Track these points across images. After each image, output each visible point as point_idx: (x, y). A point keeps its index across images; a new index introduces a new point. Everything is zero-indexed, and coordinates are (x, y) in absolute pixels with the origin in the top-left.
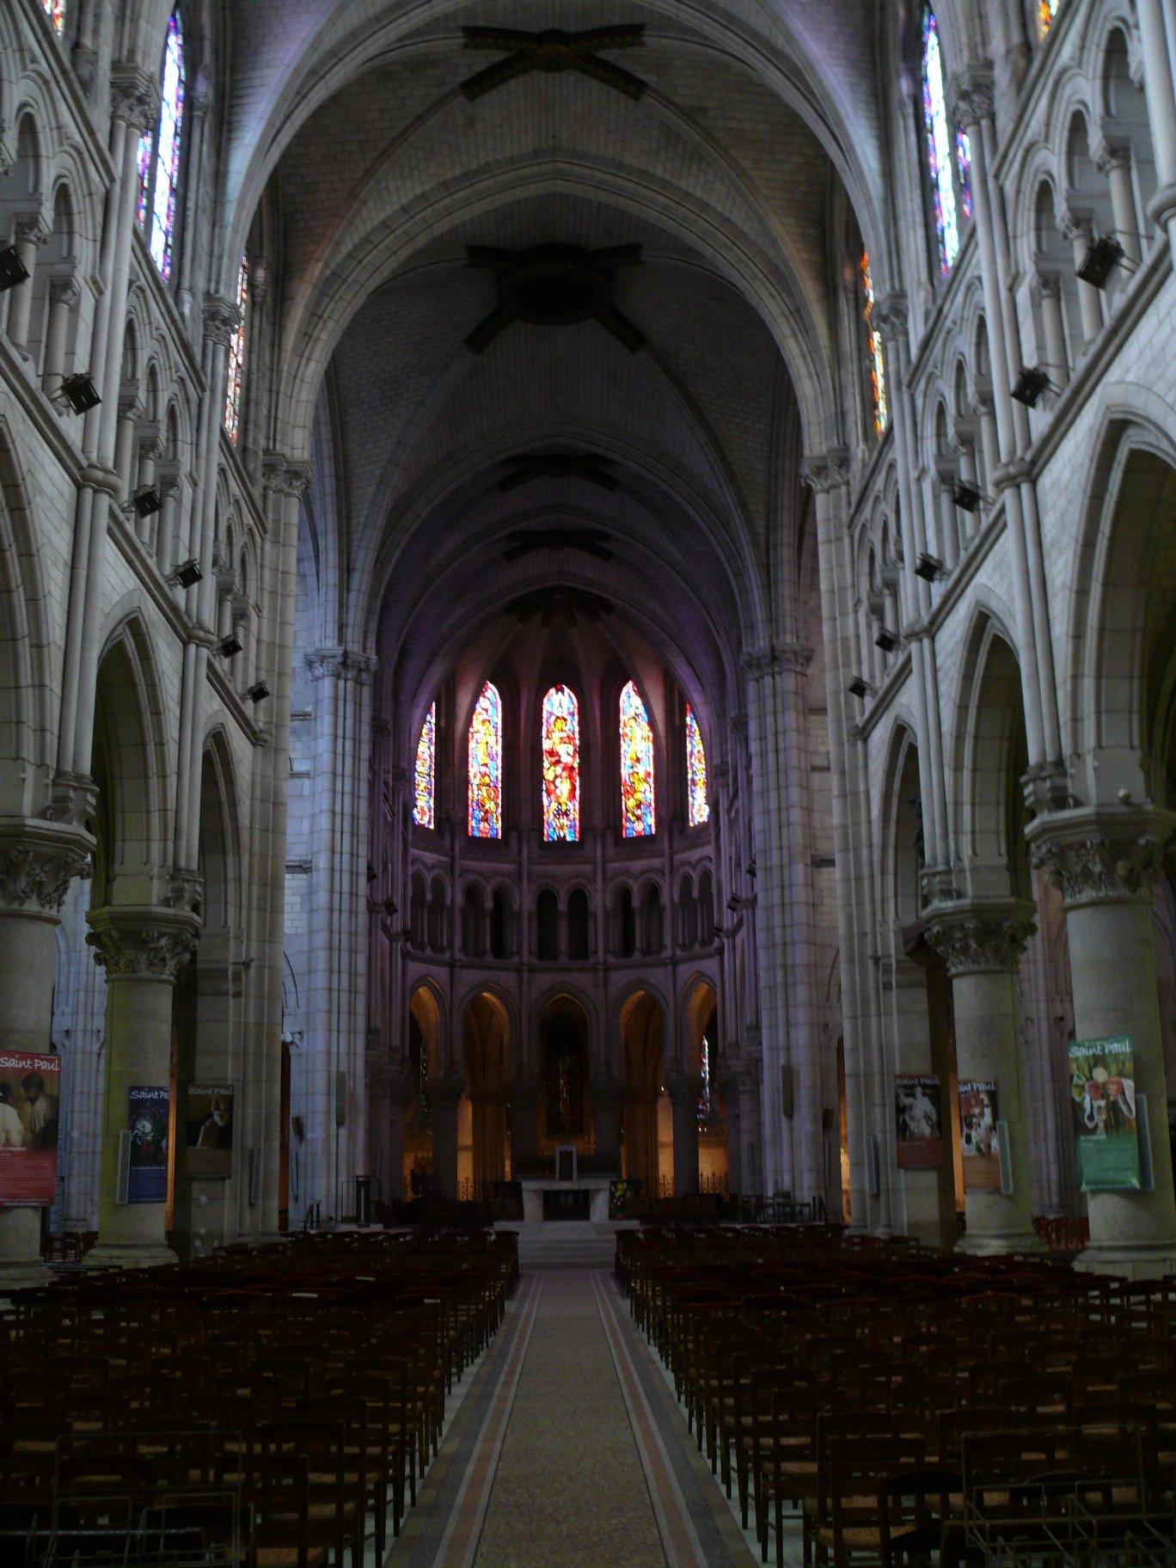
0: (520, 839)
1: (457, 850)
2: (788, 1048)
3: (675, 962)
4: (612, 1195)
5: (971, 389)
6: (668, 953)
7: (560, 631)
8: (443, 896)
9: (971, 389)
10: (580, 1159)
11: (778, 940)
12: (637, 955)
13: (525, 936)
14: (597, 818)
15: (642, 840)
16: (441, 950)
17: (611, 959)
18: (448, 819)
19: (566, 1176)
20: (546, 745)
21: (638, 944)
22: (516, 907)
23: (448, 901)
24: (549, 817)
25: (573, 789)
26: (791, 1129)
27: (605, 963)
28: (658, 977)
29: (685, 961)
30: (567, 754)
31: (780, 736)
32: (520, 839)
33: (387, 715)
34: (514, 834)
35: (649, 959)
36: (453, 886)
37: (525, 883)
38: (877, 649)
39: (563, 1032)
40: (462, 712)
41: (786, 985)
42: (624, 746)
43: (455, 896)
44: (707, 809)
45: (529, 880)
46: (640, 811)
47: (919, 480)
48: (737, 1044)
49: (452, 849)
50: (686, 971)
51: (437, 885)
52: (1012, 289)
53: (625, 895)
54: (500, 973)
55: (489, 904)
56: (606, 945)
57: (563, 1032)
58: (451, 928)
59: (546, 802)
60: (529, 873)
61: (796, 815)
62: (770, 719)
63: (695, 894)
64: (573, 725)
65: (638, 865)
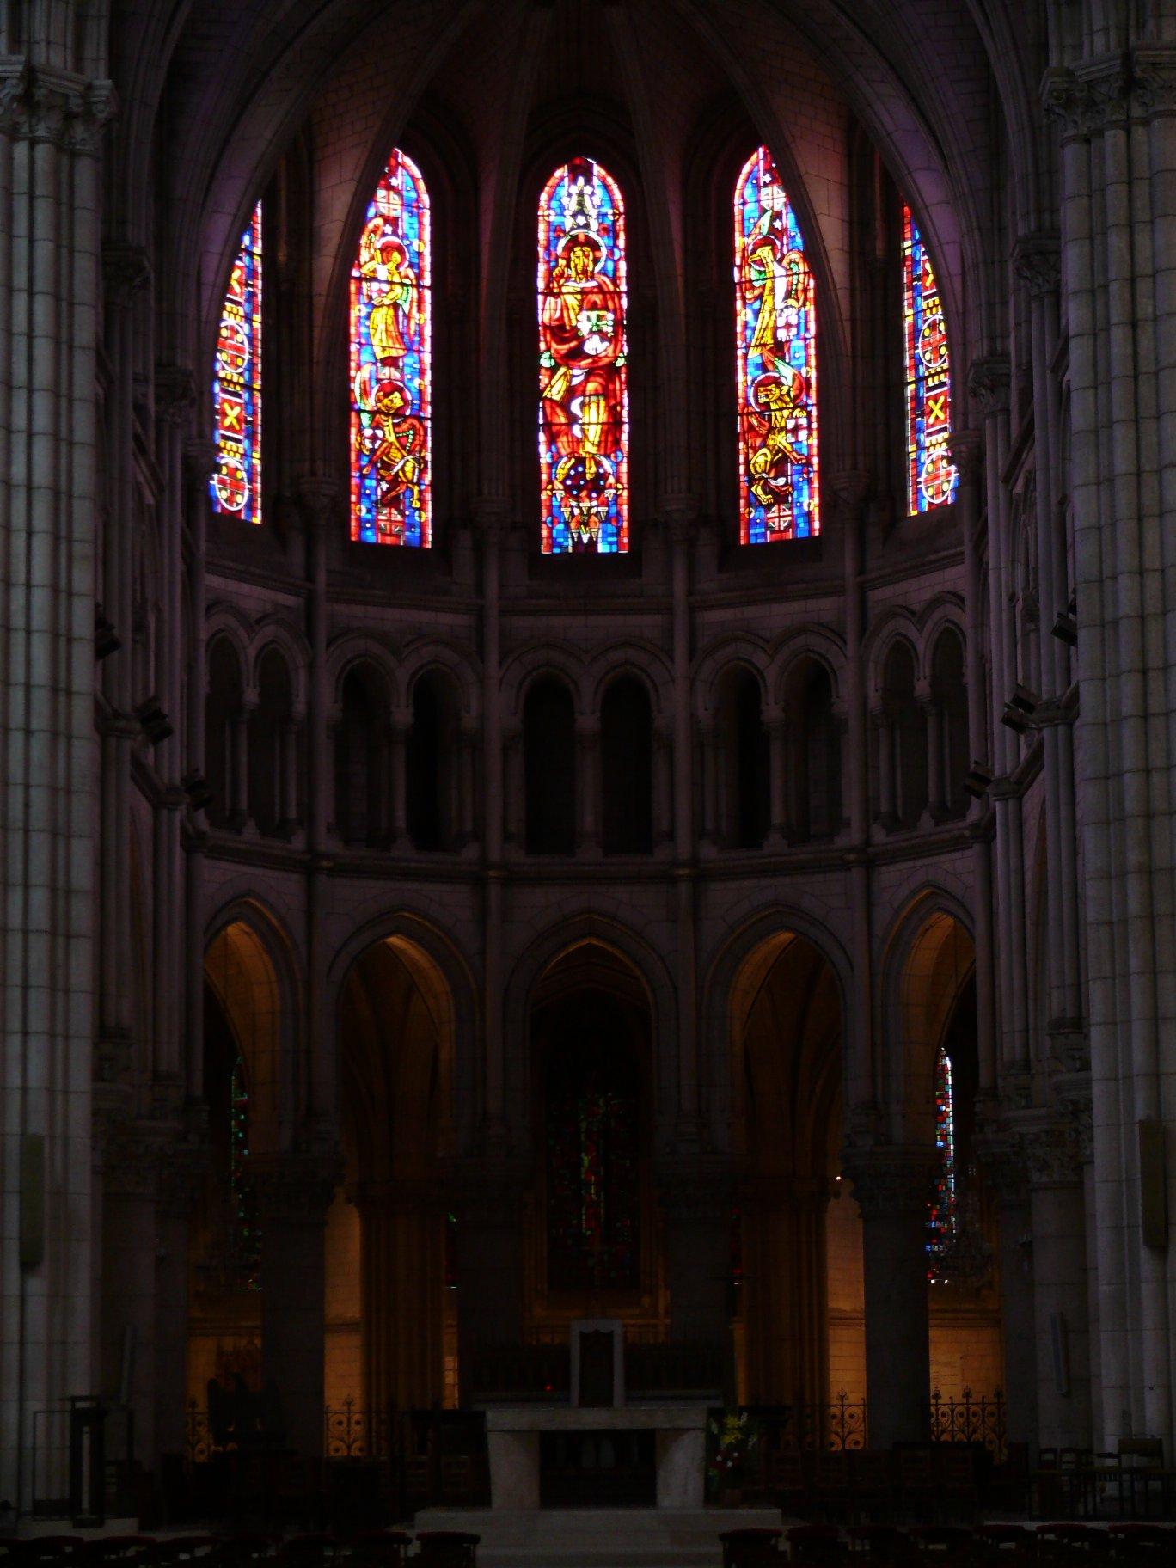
1: (322, 578)
2: (1156, 1077)
3: (870, 860)
6: (854, 836)
11: (1132, 804)
12: (775, 843)
15: (788, 551)
17: (708, 852)
19: (597, 1396)
20: (547, 311)
21: (777, 815)
22: (469, 721)
23: (300, 707)
24: (553, 493)
25: (612, 427)
26: (1163, 1281)
27: (695, 861)
29: (894, 857)
31: (1143, 286)
34: (465, 540)
36: (311, 668)
39: (589, 1030)
43: (318, 695)
46: (784, 477)
49: (310, 576)
51: (273, 666)
53: (743, 691)
55: (403, 715)
57: (589, 1030)
59: (545, 458)
63: (922, 687)
65: (779, 615)
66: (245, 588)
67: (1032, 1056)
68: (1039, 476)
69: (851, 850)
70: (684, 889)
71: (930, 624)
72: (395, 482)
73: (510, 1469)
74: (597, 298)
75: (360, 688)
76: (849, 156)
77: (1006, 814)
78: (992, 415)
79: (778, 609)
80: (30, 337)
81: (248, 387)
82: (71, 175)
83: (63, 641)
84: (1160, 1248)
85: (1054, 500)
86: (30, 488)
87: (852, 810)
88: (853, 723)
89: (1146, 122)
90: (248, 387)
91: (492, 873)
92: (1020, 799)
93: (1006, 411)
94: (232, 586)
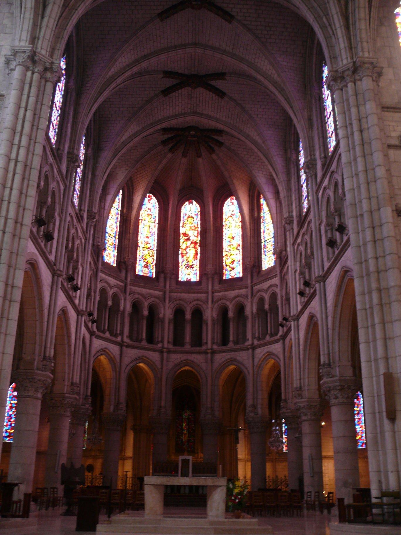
0: (165, 278)
1: (129, 279)
2: (387, 358)
3: (254, 348)
4: (229, 493)
5: (309, 251)
6: (250, 342)
7: (192, 163)
8: (118, 305)
9: (309, 251)
10: (194, 464)
11: (372, 268)
12: (231, 345)
13: (166, 333)
14: (210, 268)
15: (234, 280)
16: (116, 336)
17: (215, 347)
18: (125, 262)
19: (185, 474)
20: (182, 230)
21: (231, 338)
22: (161, 316)
23: (122, 308)
25: (196, 254)
26: (394, 432)
27: (212, 349)
28: (243, 357)
29: (260, 346)
30: (195, 236)
31: (363, 121)
32: (165, 278)
33: (95, 210)
34: (162, 276)
35: (238, 346)
36: (125, 299)
37: (167, 301)
38: (298, 296)
39: (186, 392)
40: (136, 205)
41: (381, 305)
42: (225, 230)
43: (126, 306)
44: (273, 258)
45: (170, 302)
46: (233, 264)
47: (320, 225)
48: (301, 388)
49: (126, 279)
50: (260, 352)
51: (115, 297)
52: (320, 225)
53: (224, 311)
54: (149, 352)
55: (146, 312)
56: (213, 339)
57: (186, 392)
58: (123, 324)
60: (170, 297)
61: (380, 172)
62: (354, 110)
63: (267, 307)
64: (197, 221)
65: (232, 294)
66: (110, 278)
67: (331, 361)
68: (290, 267)
69: (249, 345)
70: (209, 355)
71: (268, 292)
72: (147, 263)
73: (152, 498)
74: (194, 228)
75: (136, 306)
76: (249, 196)
77: (294, 325)
78: (289, 230)
79: (232, 292)
80: (24, 121)
81: (115, 237)
82: (45, 86)
83: (21, 209)
84: (392, 417)
85: (317, 224)
86: (16, 162)
87: (249, 336)
88: (250, 317)
89: (361, 80)
90: (115, 237)
91: (165, 350)
92: (298, 320)
93: (293, 229)
94: (107, 277)
